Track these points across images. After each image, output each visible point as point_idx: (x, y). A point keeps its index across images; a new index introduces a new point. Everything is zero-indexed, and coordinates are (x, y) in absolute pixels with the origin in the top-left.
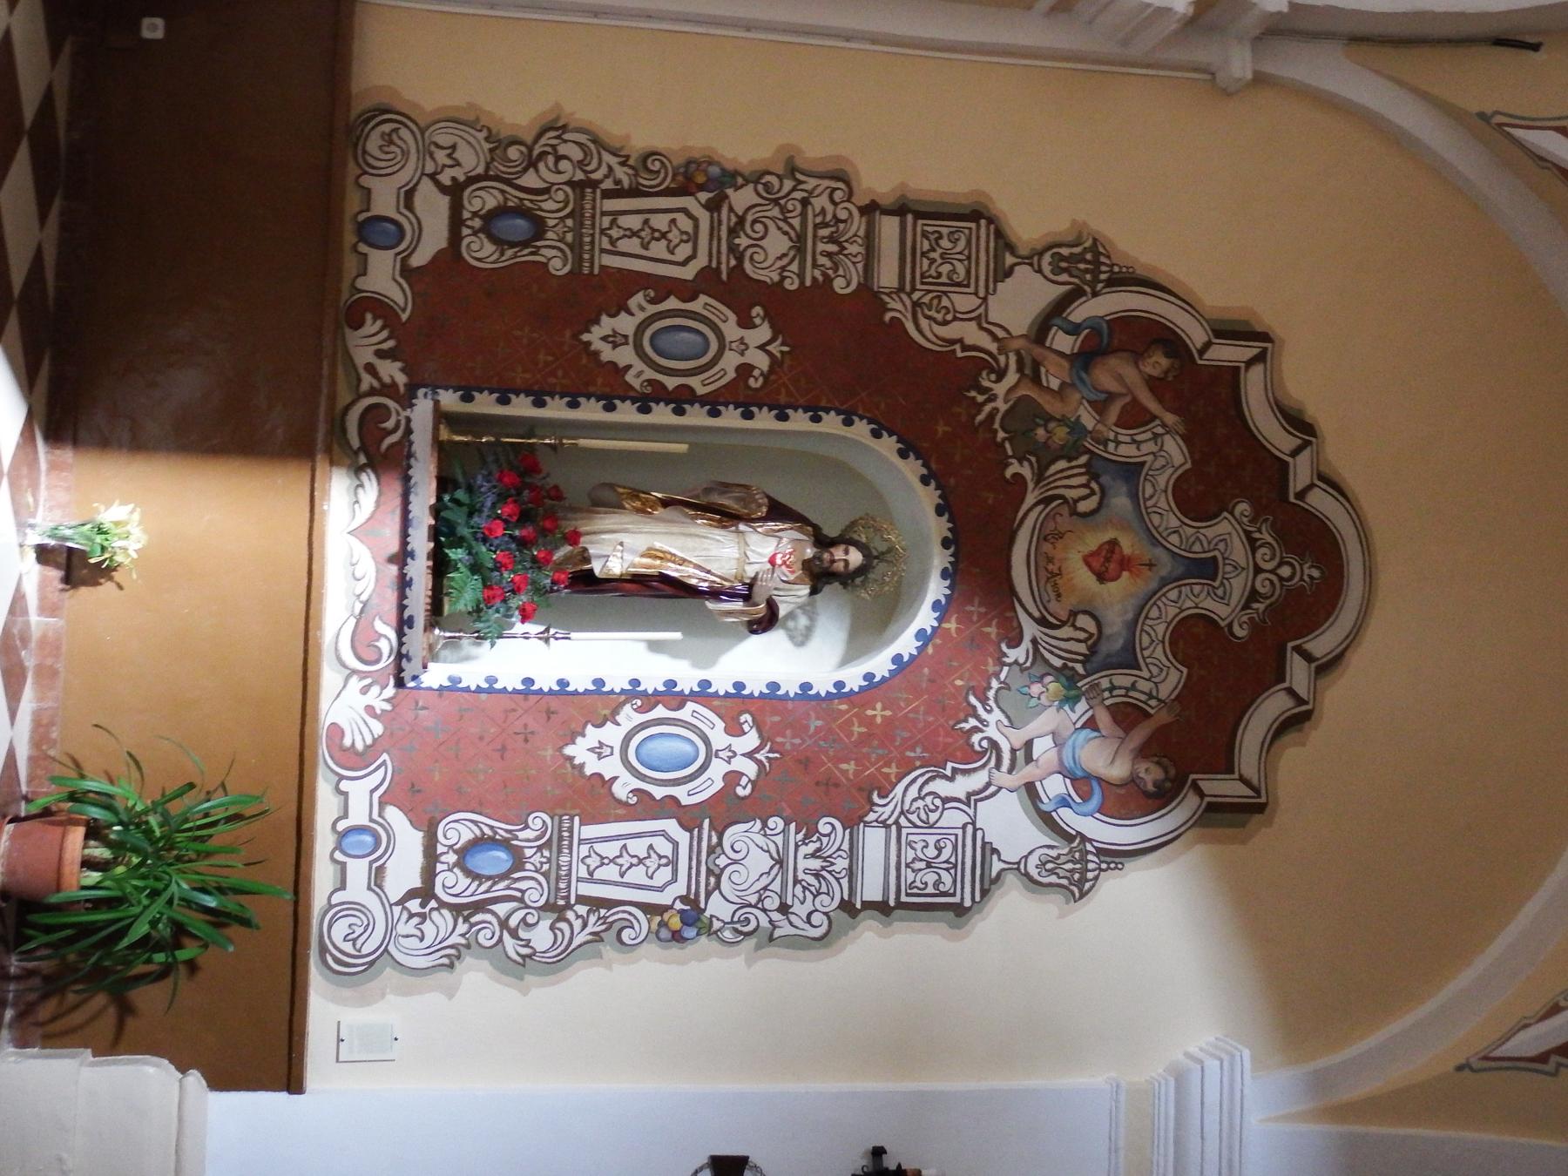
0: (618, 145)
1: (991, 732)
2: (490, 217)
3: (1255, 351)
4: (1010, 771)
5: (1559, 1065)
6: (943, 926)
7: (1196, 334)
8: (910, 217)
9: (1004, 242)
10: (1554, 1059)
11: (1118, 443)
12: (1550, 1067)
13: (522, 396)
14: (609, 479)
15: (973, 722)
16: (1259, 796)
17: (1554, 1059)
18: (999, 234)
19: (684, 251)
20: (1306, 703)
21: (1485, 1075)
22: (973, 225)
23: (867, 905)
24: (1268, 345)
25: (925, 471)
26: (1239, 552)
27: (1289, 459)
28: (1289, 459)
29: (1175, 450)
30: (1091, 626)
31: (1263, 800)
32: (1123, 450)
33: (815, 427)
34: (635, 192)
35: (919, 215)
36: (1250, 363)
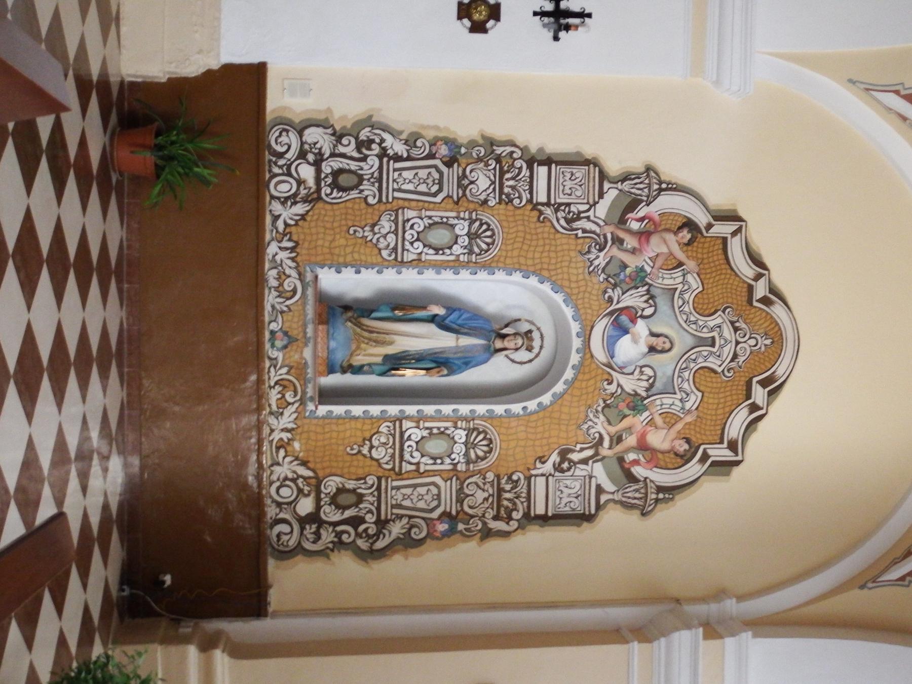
0: (322, 117)
1: (599, 428)
2: (336, 173)
3: (737, 227)
4: (610, 448)
5: (910, 582)
6: (537, 527)
7: (702, 218)
8: (553, 166)
9: (603, 176)
10: (908, 578)
11: (663, 278)
12: (906, 583)
13: (349, 268)
14: (654, 339)
15: (590, 423)
16: (737, 455)
17: (908, 578)
18: (601, 173)
19: (435, 188)
20: (762, 409)
21: (874, 590)
22: (587, 168)
23: (538, 517)
24: (743, 224)
25: (354, 269)
26: (727, 332)
27: (753, 283)
28: (753, 283)
29: (694, 281)
30: (651, 373)
31: (739, 458)
32: (666, 282)
33: (508, 278)
34: (409, 158)
35: (558, 163)
36: (734, 234)
